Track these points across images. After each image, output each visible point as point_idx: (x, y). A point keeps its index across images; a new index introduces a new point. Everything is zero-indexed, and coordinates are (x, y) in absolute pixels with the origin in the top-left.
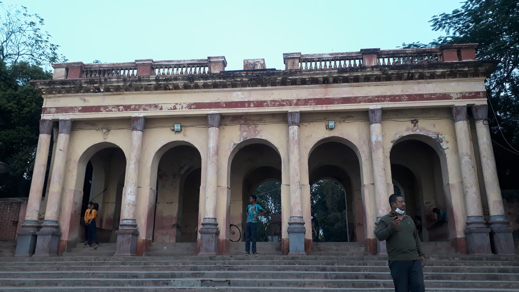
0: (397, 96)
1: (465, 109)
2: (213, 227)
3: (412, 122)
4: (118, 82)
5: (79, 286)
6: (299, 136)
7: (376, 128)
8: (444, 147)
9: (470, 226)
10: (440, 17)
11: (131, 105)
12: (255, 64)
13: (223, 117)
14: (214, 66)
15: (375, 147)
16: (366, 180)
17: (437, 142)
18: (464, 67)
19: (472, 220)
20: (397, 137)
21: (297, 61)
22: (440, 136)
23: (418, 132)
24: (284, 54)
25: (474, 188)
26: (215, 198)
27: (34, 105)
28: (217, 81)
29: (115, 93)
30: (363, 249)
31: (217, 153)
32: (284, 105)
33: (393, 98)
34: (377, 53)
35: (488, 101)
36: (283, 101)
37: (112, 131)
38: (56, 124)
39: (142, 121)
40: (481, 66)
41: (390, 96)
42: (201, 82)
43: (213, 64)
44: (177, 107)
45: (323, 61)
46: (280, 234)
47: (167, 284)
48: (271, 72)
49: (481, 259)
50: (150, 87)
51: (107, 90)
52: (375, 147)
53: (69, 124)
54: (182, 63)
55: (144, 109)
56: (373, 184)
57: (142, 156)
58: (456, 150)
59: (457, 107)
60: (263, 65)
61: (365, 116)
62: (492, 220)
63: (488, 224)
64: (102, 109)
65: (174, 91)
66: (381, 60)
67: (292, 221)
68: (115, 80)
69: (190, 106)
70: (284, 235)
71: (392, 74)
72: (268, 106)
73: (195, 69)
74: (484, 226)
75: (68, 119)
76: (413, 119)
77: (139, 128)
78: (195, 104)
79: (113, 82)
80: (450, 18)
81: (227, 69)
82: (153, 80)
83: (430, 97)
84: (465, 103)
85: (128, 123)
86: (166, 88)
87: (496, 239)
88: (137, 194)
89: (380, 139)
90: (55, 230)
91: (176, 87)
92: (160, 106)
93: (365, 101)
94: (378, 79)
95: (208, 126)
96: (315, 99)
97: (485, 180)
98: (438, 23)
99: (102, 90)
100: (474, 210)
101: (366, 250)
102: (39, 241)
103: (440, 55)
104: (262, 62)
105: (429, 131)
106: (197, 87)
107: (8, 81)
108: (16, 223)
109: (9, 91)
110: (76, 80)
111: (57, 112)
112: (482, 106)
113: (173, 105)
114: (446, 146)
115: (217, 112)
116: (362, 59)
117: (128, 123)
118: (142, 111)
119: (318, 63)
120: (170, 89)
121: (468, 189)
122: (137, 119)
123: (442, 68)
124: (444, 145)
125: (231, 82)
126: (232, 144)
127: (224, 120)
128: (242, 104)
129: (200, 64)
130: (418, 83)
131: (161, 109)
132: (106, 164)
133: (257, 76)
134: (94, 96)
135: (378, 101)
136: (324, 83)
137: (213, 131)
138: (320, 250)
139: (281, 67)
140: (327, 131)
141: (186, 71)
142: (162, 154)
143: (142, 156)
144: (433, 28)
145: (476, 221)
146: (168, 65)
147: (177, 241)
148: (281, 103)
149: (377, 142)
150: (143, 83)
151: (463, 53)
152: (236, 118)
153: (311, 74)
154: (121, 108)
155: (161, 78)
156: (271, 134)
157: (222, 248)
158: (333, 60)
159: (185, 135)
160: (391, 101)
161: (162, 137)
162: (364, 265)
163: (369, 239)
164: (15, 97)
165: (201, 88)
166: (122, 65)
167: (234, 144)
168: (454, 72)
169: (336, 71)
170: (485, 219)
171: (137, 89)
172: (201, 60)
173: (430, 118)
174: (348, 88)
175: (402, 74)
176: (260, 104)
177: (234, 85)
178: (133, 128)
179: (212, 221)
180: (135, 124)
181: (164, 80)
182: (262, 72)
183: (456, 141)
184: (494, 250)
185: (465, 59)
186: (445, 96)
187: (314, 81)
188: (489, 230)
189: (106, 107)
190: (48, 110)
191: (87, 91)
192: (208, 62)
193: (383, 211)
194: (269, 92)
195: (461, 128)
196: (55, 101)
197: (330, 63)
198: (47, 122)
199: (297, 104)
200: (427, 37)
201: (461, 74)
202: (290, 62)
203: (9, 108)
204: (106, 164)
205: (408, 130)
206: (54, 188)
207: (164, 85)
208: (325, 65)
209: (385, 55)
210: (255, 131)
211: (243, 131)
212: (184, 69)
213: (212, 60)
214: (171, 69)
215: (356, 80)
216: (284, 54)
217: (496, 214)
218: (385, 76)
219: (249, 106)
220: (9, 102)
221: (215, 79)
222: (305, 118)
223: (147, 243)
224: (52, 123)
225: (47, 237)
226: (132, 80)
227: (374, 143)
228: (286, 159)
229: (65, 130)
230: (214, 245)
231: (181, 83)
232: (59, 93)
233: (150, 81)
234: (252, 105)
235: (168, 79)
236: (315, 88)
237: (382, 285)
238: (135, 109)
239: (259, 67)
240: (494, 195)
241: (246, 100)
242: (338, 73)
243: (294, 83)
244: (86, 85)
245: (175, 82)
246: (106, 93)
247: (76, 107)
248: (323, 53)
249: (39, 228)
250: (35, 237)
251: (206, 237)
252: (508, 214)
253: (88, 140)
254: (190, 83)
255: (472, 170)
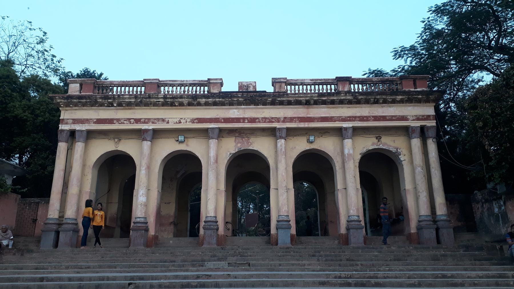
0: (365, 117)
1: (419, 129)
2: (214, 224)
3: (377, 138)
4: (130, 98)
5: (133, 268)
6: (285, 147)
7: (348, 143)
8: (402, 159)
9: (421, 223)
10: (400, 49)
11: (141, 119)
12: (248, 86)
13: (221, 130)
14: (213, 86)
15: (347, 157)
16: (339, 185)
17: (397, 155)
18: (418, 95)
19: (423, 218)
20: (365, 150)
21: (283, 85)
22: (399, 150)
23: (381, 146)
24: (273, 79)
25: (424, 192)
26: (214, 200)
27: (47, 115)
28: (217, 100)
29: (127, 108)
30: (336, 242)
31: (216, 161)
32: (273, 122)
33: (362, 119)
34: (349, 80)
35: (437, 123)
36: (273, 118)
37: (123, 141)
38: (72, 134)
39: (151, 133)
40: (431, 95)
41: (359, 117)
42: (203, 100)
43: (212, 85)
44: (182, 121)
45: (305, 85)
46: (269, 231)
47: (202, 266)
48: (263, 94)
49: (429, 248)
50: (159, 104)
51: (120, 105)
52: (347, 157)
53: (85, 134)
54: (185, 82)
55: (153, 123)
56: (345, 189)
57: (148, 162)
58: (411, 162)
59: (412, 127)
60: (255, 87)
61: (339, 132)
62: (438, 218)
63: (435, 221)
64: (115, 122)
65: (179, 107)
66: (352, 86)
67: (281, 219)
68: (128, 96)
69: (193, 121)
70: (273, 231)
71: (362, 99)
72: (259, 122)
73: (196, 88)
74: (431, 223)
75: (84, 129)
76: (377, 136)
77: (148, 139)
78: (197, 119)
79: (126, 98)
80: (408, 50)
81: (224, 89)
82: (162, 98)
83: (392, 118)
84: (418, 124)
85: (140, 134)
86: (172, 105)
87: (440, 234)
88: (147, 197)
89: (351, 152)
90: (75, 226)
91: (181, 104)
92: (167, 120)
93: (339, 121)
94: (350, 102)
95: (209, 138)
96: (298, 118)
97: (434, 186)
98: (398, 54)
99: (115, 105)
100: (425, 211)
101: (339, 243)
102: (62, 236)
103: (400, 84)
104: (254, 85)
105: (390, 146)
106: (199, 104)
107: (22, 92)
108: (35, 221)
109: (24, 102)
110: (91, 96)
111: (74, 123)
112: (432, 127)
113: (178, 119)
114: (404, 158)
115: (217, 126)
116: (337, 85)
117: (139, 134)
118: (151, 124)
119: (301, 87)
120: (175, 106)
121: (420, 194)
122: (146, 131)
123: (402, 95)
124: (402, 158)
125: (229, 101)
126: (229, 154)
127: (222, 133)
128: (237, 120)
129: (201, 84)
130: (382, 107)
131: (168, 122)
132: (117, 171)
133: (251, 97)
134: (108, 110)
135: (350, 121)
136: (306, 104)
137: (213, 143)
138: (302, 243)
139: (270, 89)
140: (308, 144)
141: (188, 90)
142: (166, 161)
143: (148, 162)
144: (394, 57)
145: (426, 219)
146: (173, 84)
147: (174, 237)
148: (271, 120)
149: (349, 155)
150: (152, 100)
151: (418, 83)
152: (231, 132)
153: (295, 97)
154: (132, 121)
155: (168, 96)
156: (262, 146)
157: (221, 241)
158: (313, 85)
159: (187, 145)
160: (360, 121)
161: (168, 147)
162: (343, 252)
163: (342, 234)
164: (29, 107)
165: (203, 106)
166: (131, 83)
167: (230, 154)
168: (411, 99)
169: (316, 95)
170: (433, 218)
171: (147, 105)
172: (202, 81)
173: (391, 135)
174: (326, 109)
175: (370, 99)
176: (253, 120)
177: (231, 104)
178: (143, 139)
179: (214, 219)
180: (145, 135)
181: (171, 98)
182: (255, 94)
183: (411, 154)
184: (439, 242)
185: (420, 87)
186: (403, 118)
187: (298, 103)
188: (435, 226)
189: (118, 120)
190: (65, 121)
191: (102, 105)
192: (208, 83)
193: (354, 211)
194: (261, 110)
195: (415, 145)
196: (72, 113)
197: (311, 87)
198: (65, 132)
199: (284, 122)
200: (390, 65)
201: (416, 100)
202: (277, 86)
203: (25, 117)
204: (117, 171)
205: (373, 144)
206: (73, 190)
207: (171, 102)
208: (307, 89)
209: (355, 82)
210: (248, 143)
211: (238, 143)
212: (187, 88)
213: (211, 81)
214: (175, 88)
215: (333, 102)
216: (273, 79)
217: (441, 214)
218: (356, 100)
219: (244, 122)
220: (24, 112)
221: (215, 98)
222: (291, 133)
223: (156, 237)
224: (69, 133)
225: (69, 232)
226: (143, 98)
227: (346, 155)
228: (274, 167)
229: (81, 140)
230: (215, 239)
231: (185, 101)
232: (75, 106)
233: (158, 98)
234: (246, 121)
235: (174, 97)
236: (298, 108)
237: (360, 265)
238: (145, 122)
239: (251, 89)
240: (440, 199)
241: (241, 117)
242: (318, 96)
243: (281, 103)
244: (101, 100)
245: (180, 100)
246: (118, 108)
247: (91, 119)
248: (305, 78)
249: (60, 225)
250: (58, 233)
251: (209, 232)
252: (450, 213)
253: (101, 148)
254: (194, 101)
255: (424, 178)
